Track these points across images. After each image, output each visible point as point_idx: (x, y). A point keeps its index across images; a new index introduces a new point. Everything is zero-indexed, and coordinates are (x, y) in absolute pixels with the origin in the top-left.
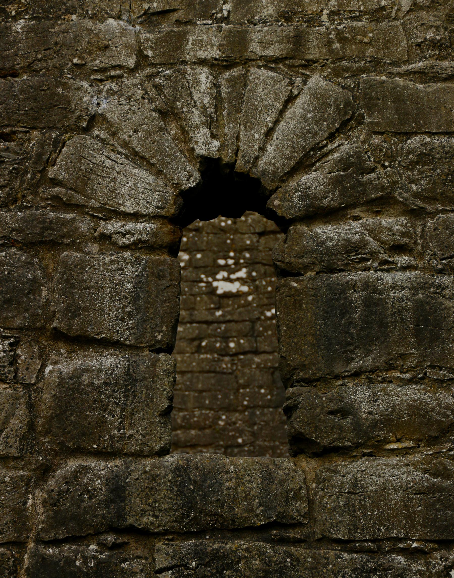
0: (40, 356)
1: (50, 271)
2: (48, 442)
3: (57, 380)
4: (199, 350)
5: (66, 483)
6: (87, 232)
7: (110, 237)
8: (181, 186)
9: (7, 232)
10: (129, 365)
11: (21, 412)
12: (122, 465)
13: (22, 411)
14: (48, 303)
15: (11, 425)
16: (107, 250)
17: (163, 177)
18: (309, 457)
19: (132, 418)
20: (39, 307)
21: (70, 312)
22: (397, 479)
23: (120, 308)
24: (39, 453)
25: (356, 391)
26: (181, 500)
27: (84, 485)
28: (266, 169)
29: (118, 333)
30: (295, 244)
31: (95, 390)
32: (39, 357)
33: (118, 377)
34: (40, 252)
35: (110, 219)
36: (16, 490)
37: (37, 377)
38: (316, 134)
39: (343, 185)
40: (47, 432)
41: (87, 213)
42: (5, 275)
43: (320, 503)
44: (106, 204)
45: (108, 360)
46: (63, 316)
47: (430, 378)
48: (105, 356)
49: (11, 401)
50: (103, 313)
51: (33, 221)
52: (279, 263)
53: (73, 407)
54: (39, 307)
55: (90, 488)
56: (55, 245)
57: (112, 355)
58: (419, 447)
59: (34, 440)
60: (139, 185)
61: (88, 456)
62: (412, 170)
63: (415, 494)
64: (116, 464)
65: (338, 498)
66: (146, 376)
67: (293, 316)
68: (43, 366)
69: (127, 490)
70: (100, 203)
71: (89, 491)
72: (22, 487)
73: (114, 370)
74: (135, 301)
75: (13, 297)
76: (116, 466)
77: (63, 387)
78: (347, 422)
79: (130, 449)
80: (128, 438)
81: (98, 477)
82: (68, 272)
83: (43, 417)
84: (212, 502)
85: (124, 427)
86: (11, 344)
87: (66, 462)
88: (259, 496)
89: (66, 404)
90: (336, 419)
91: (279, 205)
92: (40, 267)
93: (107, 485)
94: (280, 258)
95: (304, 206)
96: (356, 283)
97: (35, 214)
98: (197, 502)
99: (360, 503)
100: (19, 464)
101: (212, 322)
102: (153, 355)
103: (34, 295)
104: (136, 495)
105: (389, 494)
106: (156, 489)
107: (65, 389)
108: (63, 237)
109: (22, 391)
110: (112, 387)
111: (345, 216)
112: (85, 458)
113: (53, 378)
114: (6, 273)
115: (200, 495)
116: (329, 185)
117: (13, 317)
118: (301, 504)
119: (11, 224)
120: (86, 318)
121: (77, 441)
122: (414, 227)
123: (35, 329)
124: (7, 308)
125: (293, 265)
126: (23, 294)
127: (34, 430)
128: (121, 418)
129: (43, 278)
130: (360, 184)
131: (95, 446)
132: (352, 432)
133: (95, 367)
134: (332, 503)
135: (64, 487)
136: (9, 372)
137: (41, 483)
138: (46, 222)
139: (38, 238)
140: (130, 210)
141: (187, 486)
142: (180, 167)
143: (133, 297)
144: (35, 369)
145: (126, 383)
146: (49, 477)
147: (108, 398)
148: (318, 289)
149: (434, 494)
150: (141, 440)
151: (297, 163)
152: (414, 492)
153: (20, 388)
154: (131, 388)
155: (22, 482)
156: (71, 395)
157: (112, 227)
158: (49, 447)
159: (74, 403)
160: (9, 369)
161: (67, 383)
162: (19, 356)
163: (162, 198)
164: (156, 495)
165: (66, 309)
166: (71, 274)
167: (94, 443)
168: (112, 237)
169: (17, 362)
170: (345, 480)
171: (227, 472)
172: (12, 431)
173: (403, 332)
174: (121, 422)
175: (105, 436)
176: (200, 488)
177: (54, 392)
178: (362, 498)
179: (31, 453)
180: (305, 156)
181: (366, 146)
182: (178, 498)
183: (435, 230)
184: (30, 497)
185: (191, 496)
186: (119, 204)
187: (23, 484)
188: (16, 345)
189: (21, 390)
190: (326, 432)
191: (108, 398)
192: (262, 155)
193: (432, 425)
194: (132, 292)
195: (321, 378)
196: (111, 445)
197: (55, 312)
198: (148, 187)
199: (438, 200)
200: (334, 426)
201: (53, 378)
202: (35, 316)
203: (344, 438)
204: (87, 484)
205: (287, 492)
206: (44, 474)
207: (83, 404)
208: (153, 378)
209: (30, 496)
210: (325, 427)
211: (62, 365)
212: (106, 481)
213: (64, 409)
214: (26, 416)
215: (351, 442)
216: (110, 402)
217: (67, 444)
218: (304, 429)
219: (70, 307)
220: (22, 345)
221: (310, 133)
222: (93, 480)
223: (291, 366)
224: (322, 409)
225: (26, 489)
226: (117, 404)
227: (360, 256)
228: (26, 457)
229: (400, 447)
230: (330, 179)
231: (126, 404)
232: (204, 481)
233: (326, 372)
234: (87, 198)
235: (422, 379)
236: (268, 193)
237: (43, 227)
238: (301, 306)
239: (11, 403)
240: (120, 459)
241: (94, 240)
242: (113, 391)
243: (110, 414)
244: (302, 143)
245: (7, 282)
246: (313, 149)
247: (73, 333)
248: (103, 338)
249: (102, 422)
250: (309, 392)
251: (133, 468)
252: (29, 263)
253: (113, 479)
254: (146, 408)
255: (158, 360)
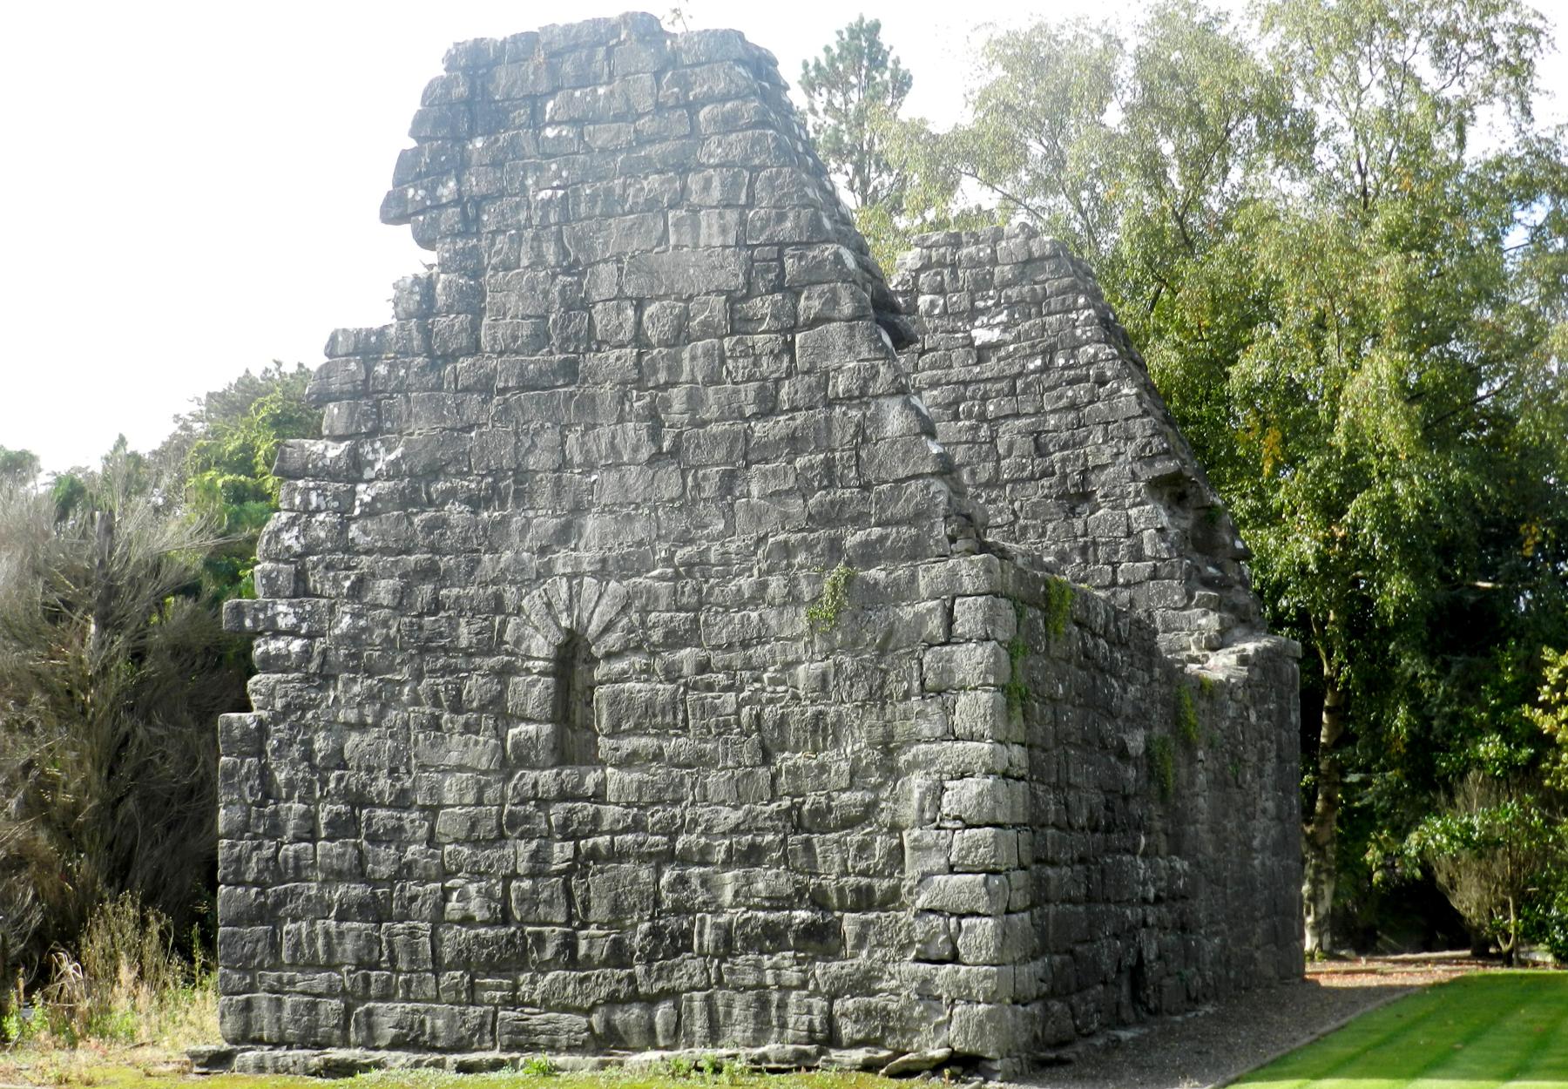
4: (956, 417)
101: (970, 382)
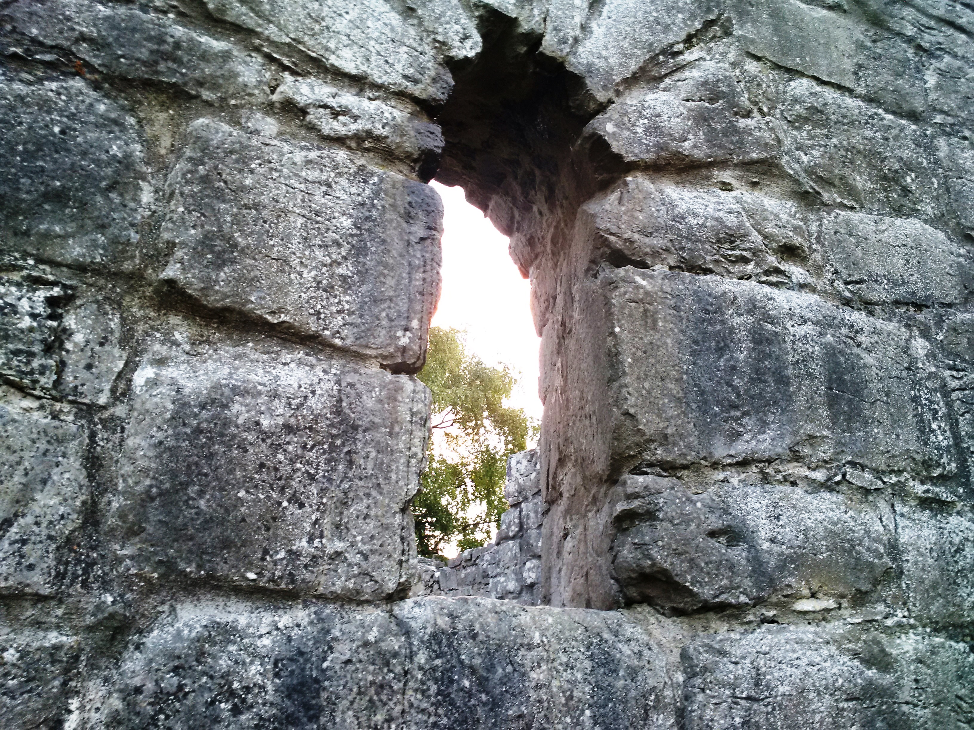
0: (125, 340)
1: (163, 151)
2: (132, 558)
3: (170, 406)
5: (176, 670)
6: (256, 87)
7: (303, 112)
8: (449, 49)
9: (67, 39)
10: (340, 391)
11: (67, 475)
12: (311, 623)
13: (70, 473)
14: (154, 223)
15: (36, 508)
16: (294, 136)
17: (415, 22)
18: (663, 614)
19: (341, 513)
20: (132, 225)
21: (212, 252)
22: (819, 670)
23: (325, 265)
24: (105, 584)
25: (746, 495)
26: (446, 715)
27: (222, 677)
28: (593, 63)
29: (319, 319)
30: (638, 208)
31: (264, 440)
32: (120, 342)
33: (316, 417)
34: (141, 103)
35: (305, 74)
36: (33, 685)
37: (113, 391)
38: (667, 28)
39: (709, 125)
40: (132, 532)
41: (257, 49)
42: (54, 135)
43: (701, 718)
44: (300, 43)
45: (295, 374)
46: (193, 257)
47: (850, 483)
48: (284, 364)
49: (42, 445)
50: (287, 268)
51: (134, 30)
52: (612, 238)
53: (206, 475)
54: (132, 225)
55: (236, 685)
56: (180, 97)
57: (300, 363)
58: (840, 608)
59: (93, 548)
60: (369, 23)
61: (229, 597)
62: (798, 129)
63: (847, 700)
64: (296, 618)
65: (731, 708)
66: (377, 420)
67: (641, 338)
68: (131, 366)
69: (325, 689)
70: (287, 35)
71: (232, 693)
72: (54, 678)
73: (306, 397)
74: (358, 255)
75: (70, 189)
76: (298, 626)
77: (185, 425)
78: (738, 554)
79: (333, 584)
80: (330, 558)
81: (255, 655)
82: (210, 164)
83: (123, 493)
84: (508, 720)
85: (322, 532)
86: (51, 302)
87: (173, 610)
88: (591, 701)
89: (189, 466)
90: (719, 546)
91: (614, 134)
92: (140, 137)
93: (277, 675)
94: (614, 229)
95: (654, 146)
96: (735, 298)
97: (139, 17)
98: (478, 720)
99: (767, 719)
100: (48, 614)
102: (389, 376)
103: (121, 195)
104: (346, 703)
105: (810, 702)
106: (391, 687)
107: (188, 430)
108: (201, 84)
109: (74, 422)
110: (301, 436)
111: (708, 178)
112: (220, 601)
113: (157, 400)
114: (57, 130)
115: (485, 704)
116: (689, 120)
117: (64, 237)
118: (665, 719)
119: (78, 24)
120: (249, 272)
121: (209, 561)
122: (805, 220)
123: (117, 275)
124: (53, 211)
125: (635, 245)
126: (97, 186)
127: (96, 524)
128: (318, 510)
129: (147, 164)
130: (736, 131)
131: (251, 576)
132: (750, 576)
133: (264, 385)
134: (721, 718)
135: (170, 681)
136: (43, 370)
137: (103, 663)
138: (165, 42)
139: (143, 72)
140: (350, 68)
141: (457, 682)
142: (449, 13)
143: (353, 246)
144: (110, 370)
145: (334, 431)
146: (126, 647)
147: (292, 462)
148: (680, 298)
149: (872, 700)
150: (359, 565)
151: (641, 68)
152: (844, 697)
153: (69, 413)
154: (343, 444)
155: (53, 663)
156: (202, 447)
157: (307, 90)
158: (133, 571)
159: (210, 465)
160: (43, 361)
161: (196, 416)
162: (67, 333)
163: (415, 61)
164: (391, 704)
165: (201, 243)
166: (216, 168)
167: (250, 566)
168: (308, 113)
169: (61, 347)
170: (740, 672)
171: (530, 647)
172: (37, 524)
173: (812, 398)
174: (316, 521)
175: (277, 553)
176: (483, 684)
177: (160, 436)
178: (770, 709)
179: (85, 584)
180: (652, 58)
181: (738, 72)
182: (441, 711)
183: (836, 233)
184: (72, 707)
185: (465, 704)
186: (327, 49)
187: (56, 669)
188: (65, 305)
189: (71, 418)
190: (708, 573)
191: (292, 462)
192: (585, 39)
193: (862, 571)
194: (352, 235)
195: (693, 463)
196: (291, 574)
197: (174, 244)
198: (387, 31)
199: (834, 186)
200: (721, 562)
201: (157, 400)
202: (119, 247)
203: (739, 587)
204: (228, 673)
205: (644, 696)
206: (113, 638)
207: (231, 471)
208: (392, 427)
209: (74, 703)
210: (706, 563)
211: (179, 371)
212: (276, 665)
213: (183, 478)
214: (81, 487)
215: (748, 596)
216: (295, 471)
217: (182, 565)
218: (672, 564)
219: (212, 240)
220: (80, 307)
221: (659, 24)
222: (244, 663)
223: (644, 434)
224: (698, 526)
225: (65, 684)
226: (312, 477)
227: (738, 252)
228: (70, 595)
229: (818, 609)
230: (690, 110)
231: (330, 480)
232: (491, 668)
233: (702, 455)
234: (260, 17)
235: (838, 483)
236: (593, 106)
237: (158, 51)
238: (655, 322)
239: (41, 450)
240: (306, 606)
241: (269, 108)
242: (304, 447)
243: (294, 499)
244: (647, 36)
245: (57, 152)
246: (663, 52)
247: (213, 300)
248: (284, 322)
249: (274, 519)
250: (672, 488)
251: (338, 634)
252: (115, 122)
253: (291, 660)
254: (374, 493)
255: (399, 389)
